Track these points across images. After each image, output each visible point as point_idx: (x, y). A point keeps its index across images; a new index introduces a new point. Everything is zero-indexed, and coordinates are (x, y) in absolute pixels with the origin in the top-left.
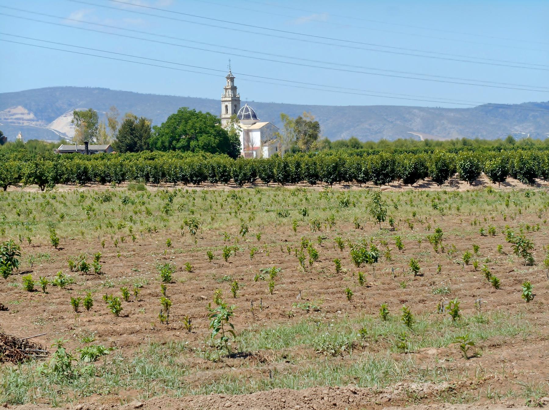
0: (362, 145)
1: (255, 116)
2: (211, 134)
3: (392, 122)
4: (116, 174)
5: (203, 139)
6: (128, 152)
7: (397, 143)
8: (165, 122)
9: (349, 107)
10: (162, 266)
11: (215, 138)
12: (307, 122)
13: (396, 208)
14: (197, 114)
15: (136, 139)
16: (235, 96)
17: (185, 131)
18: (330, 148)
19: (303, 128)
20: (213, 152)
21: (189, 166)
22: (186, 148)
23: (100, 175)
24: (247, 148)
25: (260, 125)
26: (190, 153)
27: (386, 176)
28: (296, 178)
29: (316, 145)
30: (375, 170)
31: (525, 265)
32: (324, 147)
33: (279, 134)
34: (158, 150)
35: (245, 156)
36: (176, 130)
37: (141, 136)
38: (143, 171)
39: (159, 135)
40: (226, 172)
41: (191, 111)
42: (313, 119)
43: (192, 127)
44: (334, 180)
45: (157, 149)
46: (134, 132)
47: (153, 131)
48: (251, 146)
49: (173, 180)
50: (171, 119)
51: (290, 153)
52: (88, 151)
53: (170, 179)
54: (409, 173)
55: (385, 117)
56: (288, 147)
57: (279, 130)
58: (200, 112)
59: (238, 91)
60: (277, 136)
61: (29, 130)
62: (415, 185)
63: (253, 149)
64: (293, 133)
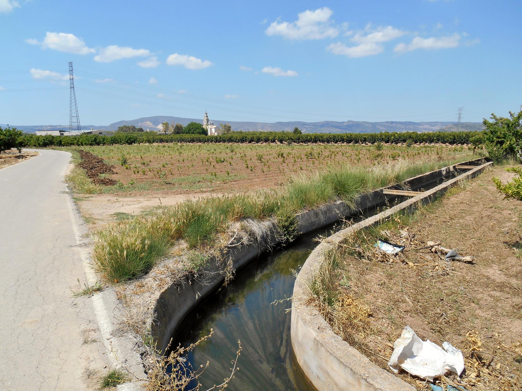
1: (213, 124)
5: (197, 131)
22: (193, 133)
24: (211, 133)
47: (184, 128)
51: (223, 134)
61: (151, 128)
63: (212, 133)
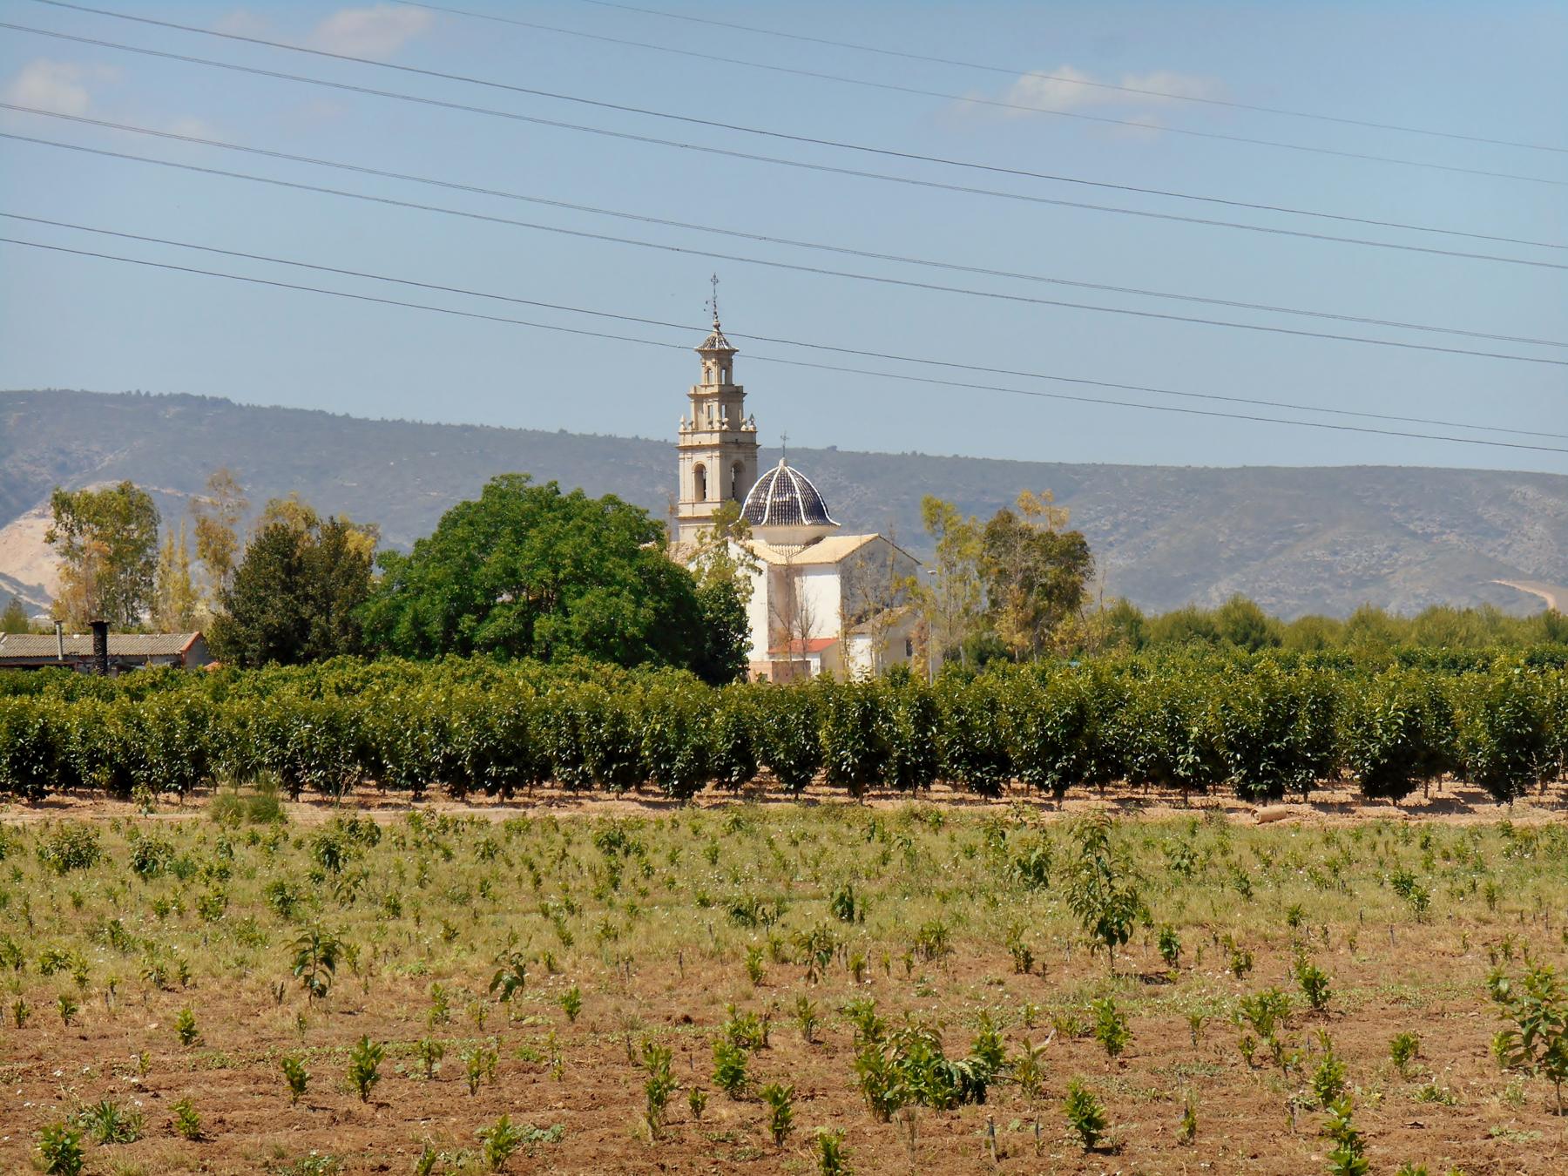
0: (1279, 633)
1: (817, 511)
2: (623, 584)
3: (1427, 537)
4: (172, 755)
5: (588, 607)
6: (272, 662)
7: (1429, 626)
8: (429, 538)
9: (1244, 471)
10: (92, 1115)
11: (639, 604)
12: (1035, 533)
13: (1245, 891)
14: (563, 505)
15: (306, 611)
16: (735, 425)
17: (513, 573)
18: (1139, 644)
19: (1019, 559)
20: (628, 662)
21: (472, 719)
22: (515, 645)
23: (111, 757)
24: (781, 640)
25: (839, 545)
26: (530, 667)
27: (1288, 761)
28: (916, 766)
29: (1074, 632)
30: (1237, 736)
31: (1556, 1113)
32: (1110, 642)
33: (914, 583)
34: (396, 653)
35: (776, 675)
36: (476, 569)
37: (328, 596)
38: (283, 743)
39: (404, 590)
40: (626, 742)
41: (540, 493)
42: (1061, 522)
43: (544, 554)
44: (1071, 777)
45: (395, 650)
46: (300, 579)
47: (377, 575)
48: (797, 634)
49: (411, 776)
50: (455, 522)
52: (103, 659)
53: (398, 775)
54: (1385, 752)
55: (1398, 516)
56: (955, 640)
57: (918, 569)
58: (578, 496)
59: (749, 406)
60: (912, 594)
62: (1411, 799)
63: (807, 647)
64: (978, 583)
